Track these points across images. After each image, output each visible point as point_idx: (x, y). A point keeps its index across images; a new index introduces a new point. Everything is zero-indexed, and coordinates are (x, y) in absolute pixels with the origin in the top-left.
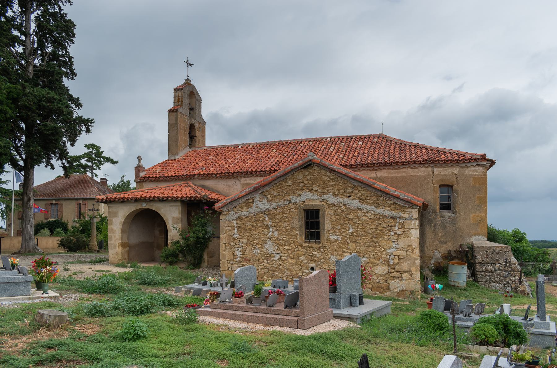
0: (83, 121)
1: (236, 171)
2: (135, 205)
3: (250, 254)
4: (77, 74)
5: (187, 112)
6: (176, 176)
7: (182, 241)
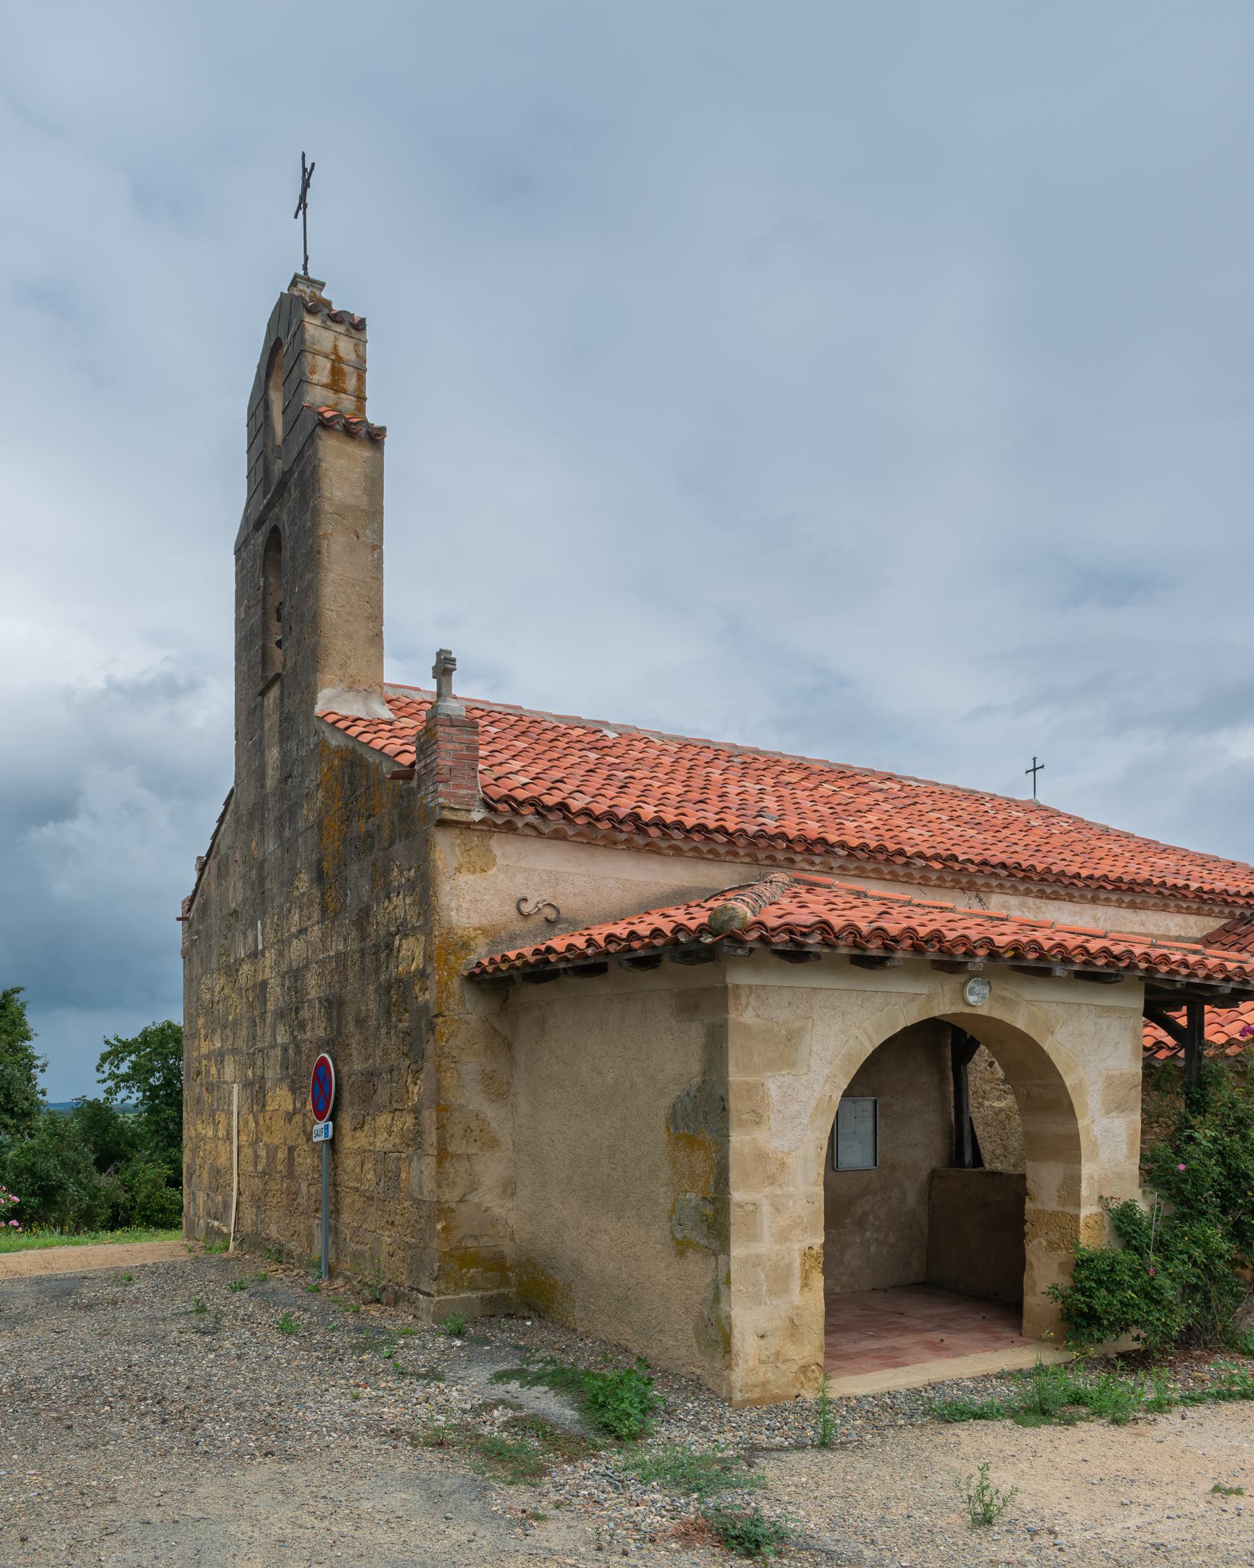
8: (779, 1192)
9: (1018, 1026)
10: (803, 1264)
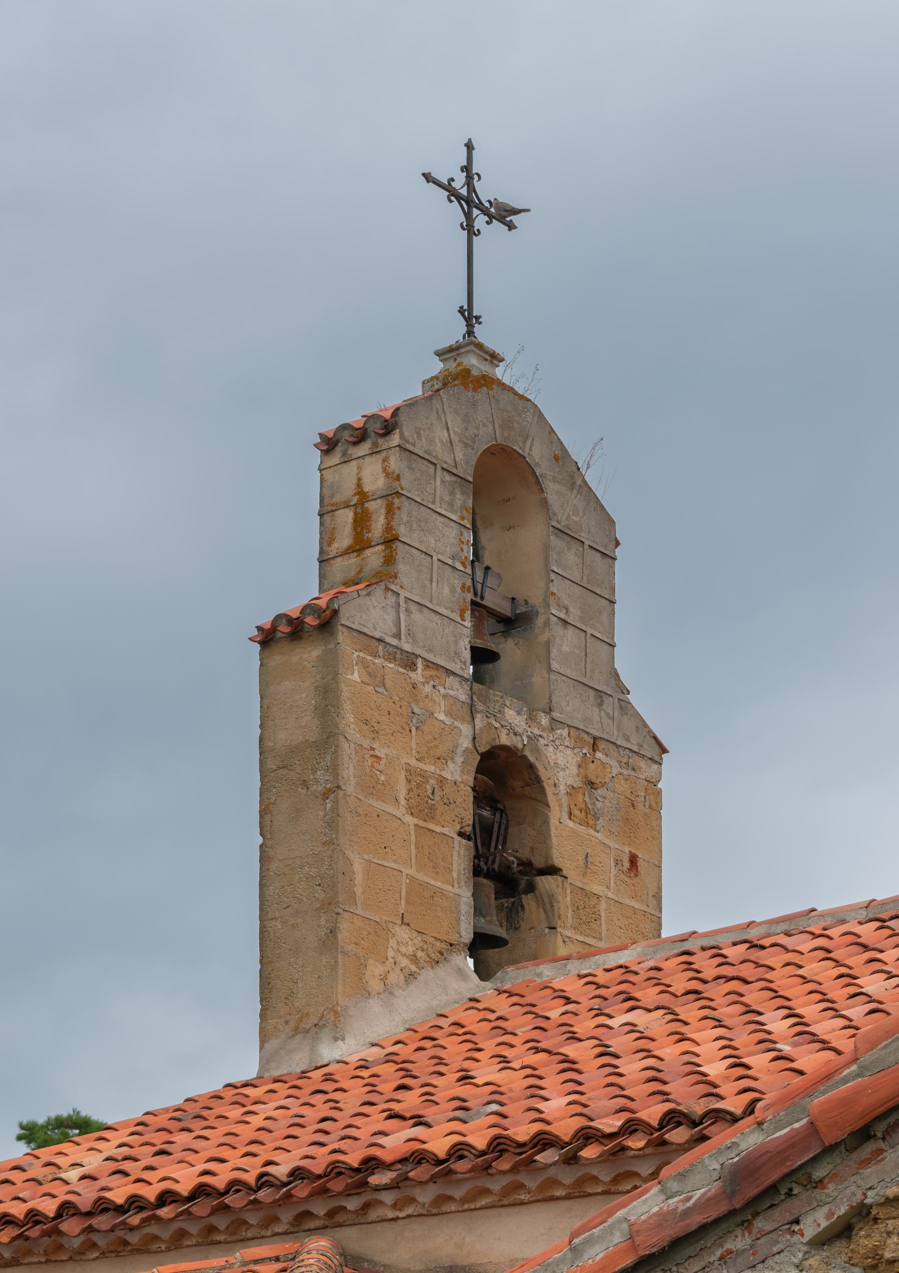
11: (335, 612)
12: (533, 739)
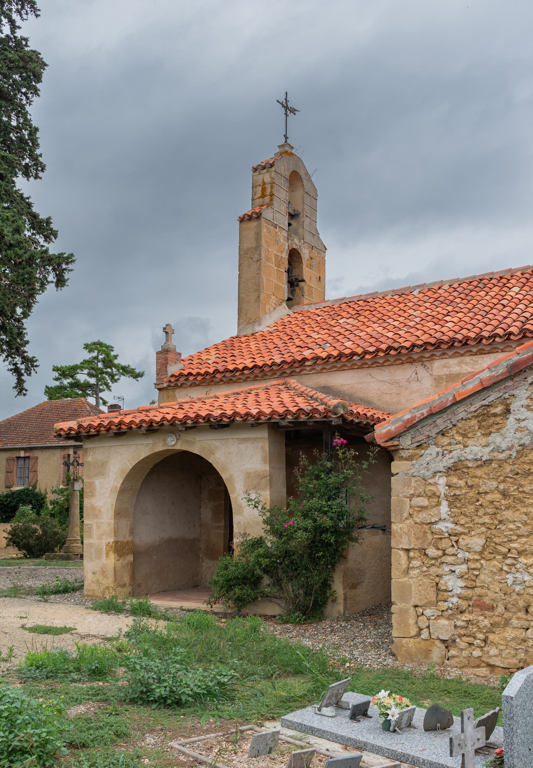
0: (49, 260)
1: (420, 343)
2: (149, 441)
3: (496, 587)
4: (45, 166)
5: (284, 221)
6: (255, 366)
7: (270, 541)
8: (99, 521)
9: (195, 453)
10: (106, 549)
11: (261, 214)
12: (300, 246)
